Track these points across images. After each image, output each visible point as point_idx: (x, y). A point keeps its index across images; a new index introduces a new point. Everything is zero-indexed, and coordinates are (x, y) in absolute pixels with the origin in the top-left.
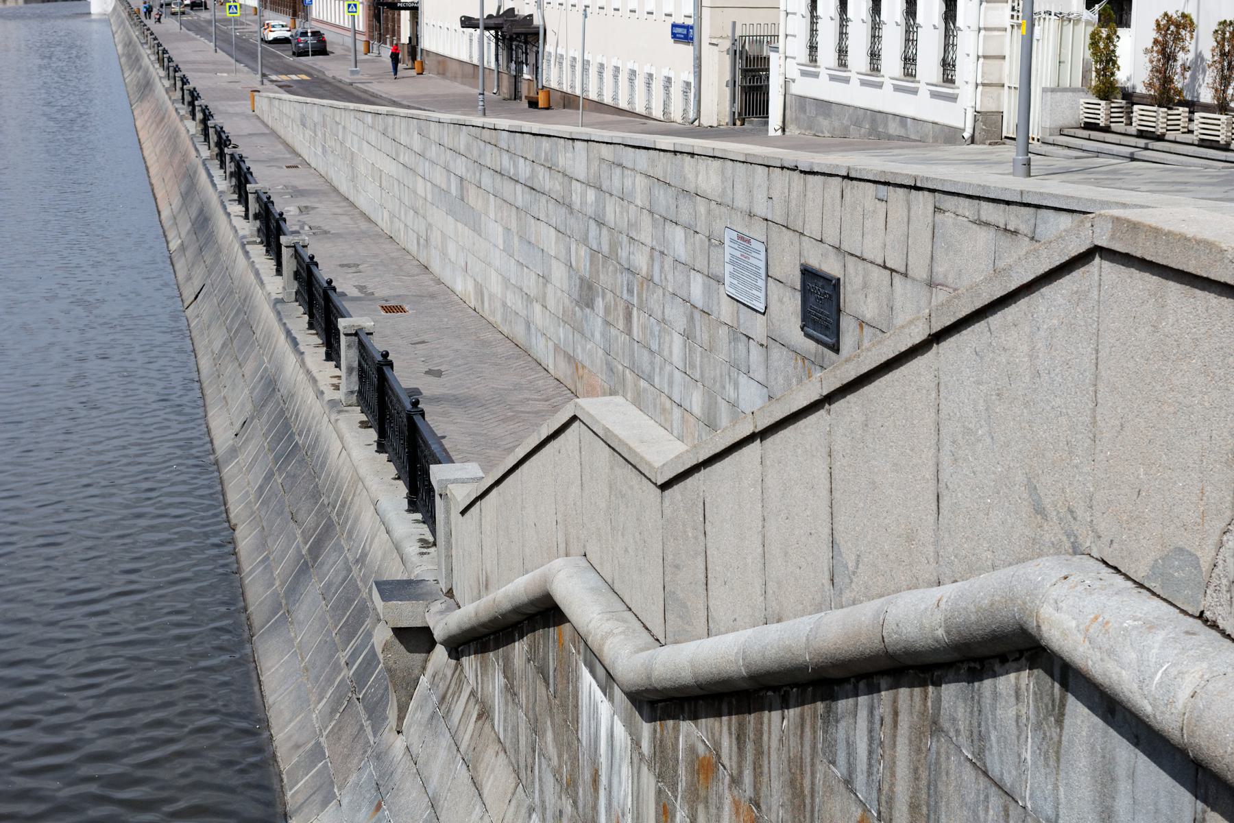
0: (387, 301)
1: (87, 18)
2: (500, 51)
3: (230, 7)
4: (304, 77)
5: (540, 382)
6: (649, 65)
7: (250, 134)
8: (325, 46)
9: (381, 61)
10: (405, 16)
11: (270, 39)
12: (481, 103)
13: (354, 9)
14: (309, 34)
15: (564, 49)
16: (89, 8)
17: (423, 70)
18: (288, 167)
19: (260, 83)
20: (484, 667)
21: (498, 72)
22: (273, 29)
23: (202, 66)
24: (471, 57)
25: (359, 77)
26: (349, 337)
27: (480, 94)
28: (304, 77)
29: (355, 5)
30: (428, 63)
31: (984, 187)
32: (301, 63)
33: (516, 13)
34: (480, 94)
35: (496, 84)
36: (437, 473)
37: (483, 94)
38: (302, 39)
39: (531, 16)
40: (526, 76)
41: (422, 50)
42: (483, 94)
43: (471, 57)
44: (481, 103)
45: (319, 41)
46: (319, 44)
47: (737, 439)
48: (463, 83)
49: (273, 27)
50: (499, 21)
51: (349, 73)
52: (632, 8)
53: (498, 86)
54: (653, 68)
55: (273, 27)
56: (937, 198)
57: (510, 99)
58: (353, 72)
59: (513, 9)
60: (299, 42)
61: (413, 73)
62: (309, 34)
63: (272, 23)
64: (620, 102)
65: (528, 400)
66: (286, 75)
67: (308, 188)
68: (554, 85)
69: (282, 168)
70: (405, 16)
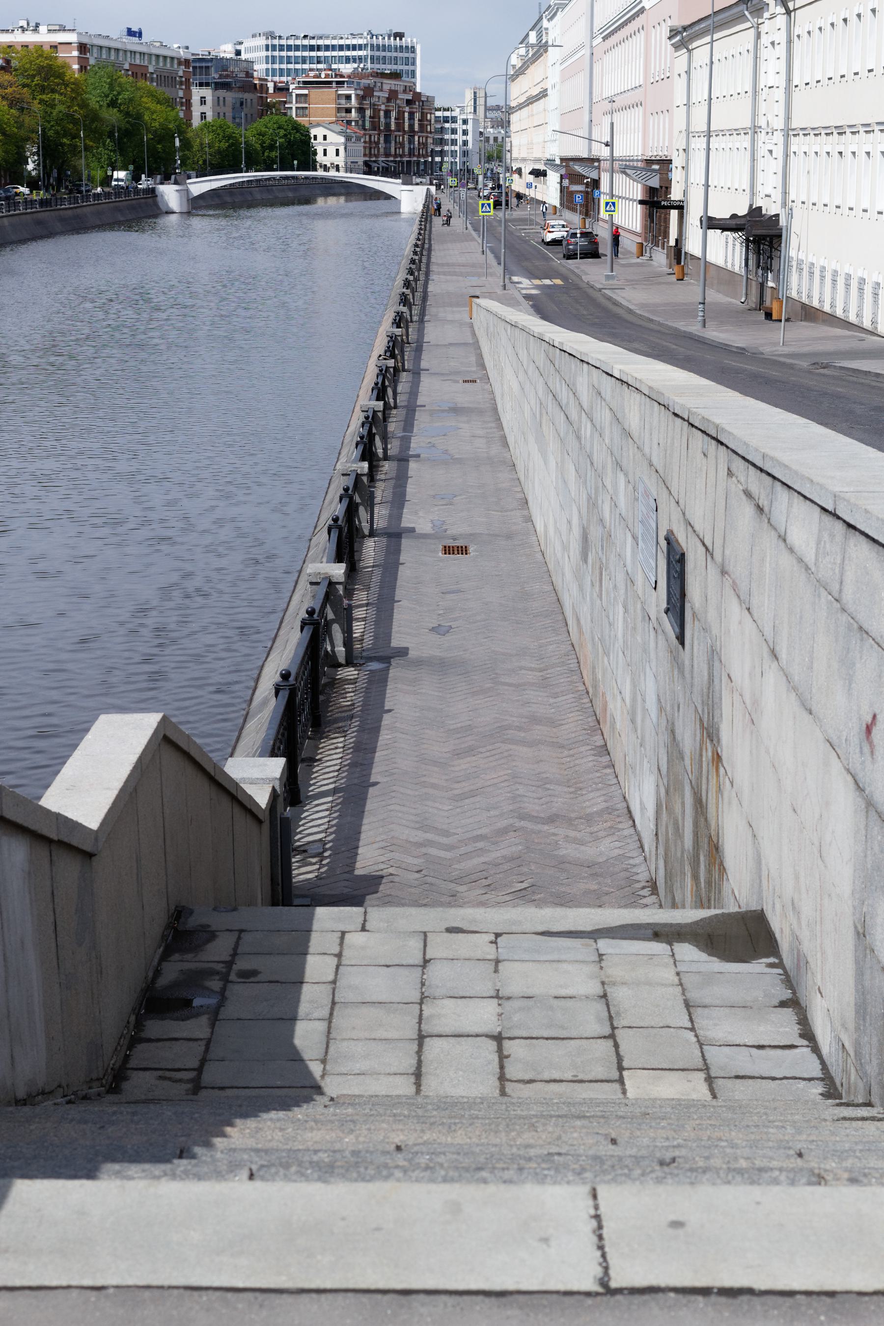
0: (455, 539)
1: (396, 217)
2: (751, 255)
3: (483, 205)
4: (558, 282)
5: (551, 648)
6: (877, 272)
7: (451, 344)
8: (597, 248)
9: (651, 265)
10: (674, 214)
11: (549, 240)
12: (701, 314)
13: (613, 208)
14: (578, 235)
15: (804, 254)
16: (400, 208)
17: (684, 275)
18: (465, 381)
19: (501, 288)
20: (747, 905)
21: (747, 278)
22: (551, 230)
23: (457, 269)
24: (726, 262)
25: (615, 282)
26: (314, 587)
27: (700, 303)
28: (558, 282)
29: (614, 204)
30: (690, 267)
31: (746, 444)
32: (564, 267)
33: (764, 212)
34: (700, 303)
35: (744, 292)
36: (853, 685)
37: (704, 303)
38: (573, 240)
39: (777, 215)
40: (771, 284)
41: (686, 253)
42: (704, 303)
43: (726, 262)
44: (701, 314)
45: (590, 242)
46: (590, 247)
47: (224, 784)
48: (718, 291)
49: (553, 227)
50: (742, 221)
51: (604, 278)
52: (864, 207)
53: (747, 294)
54: (881, 276)
55: (553, 227)
56: (383, 477)
57: (756, 309)
58: (608, 277)
59: (760, 208)
60: (568, 244)
61: (673, 278)
62: (578, 235)
63: (552, 223)
64: (850, 315)
65: (521, 668)
66: (540, 279)
67: (471, 405)
68: (794, 295)
69: (457, 382)
70: (674, 214)
